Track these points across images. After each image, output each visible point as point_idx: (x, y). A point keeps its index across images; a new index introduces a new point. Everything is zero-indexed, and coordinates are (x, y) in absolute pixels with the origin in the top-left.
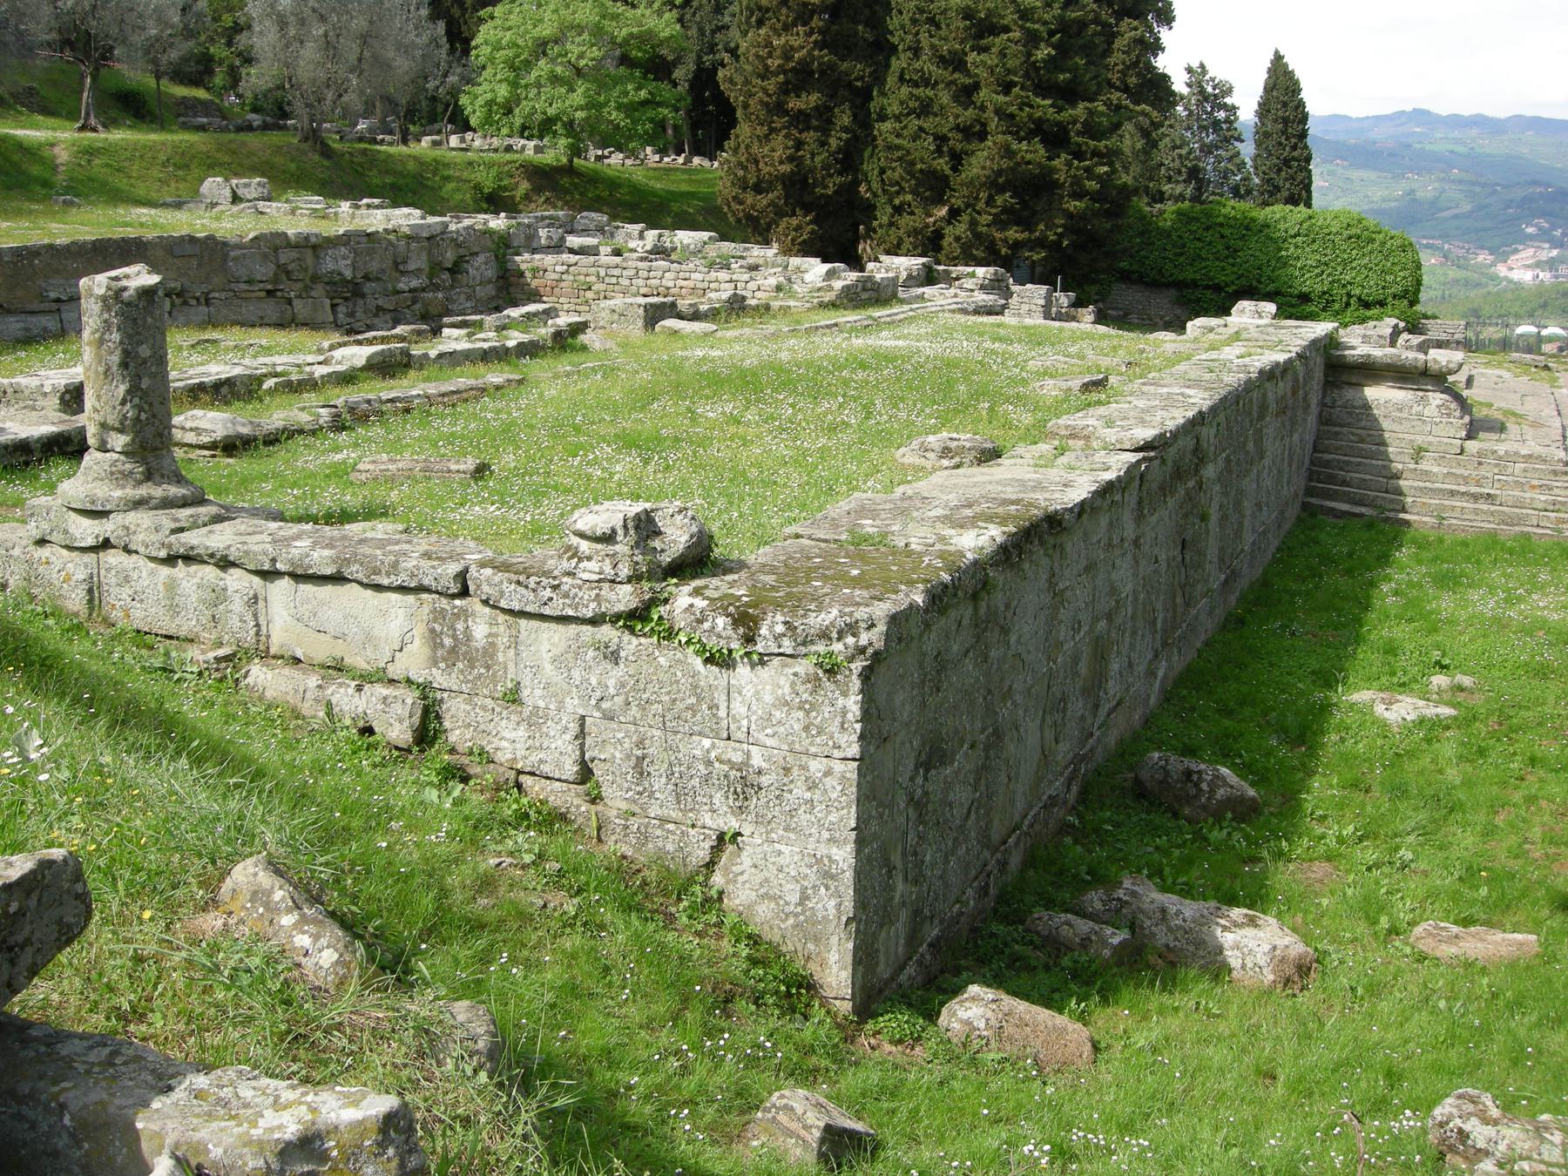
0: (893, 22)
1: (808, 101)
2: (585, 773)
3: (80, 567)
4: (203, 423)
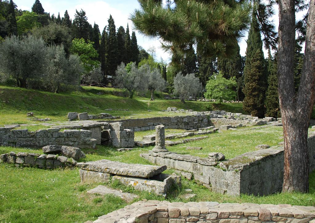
0: (268, 81)
1: (256, 93)
2: (210, 183)
3: (154, 158)
4: (168, 142)
